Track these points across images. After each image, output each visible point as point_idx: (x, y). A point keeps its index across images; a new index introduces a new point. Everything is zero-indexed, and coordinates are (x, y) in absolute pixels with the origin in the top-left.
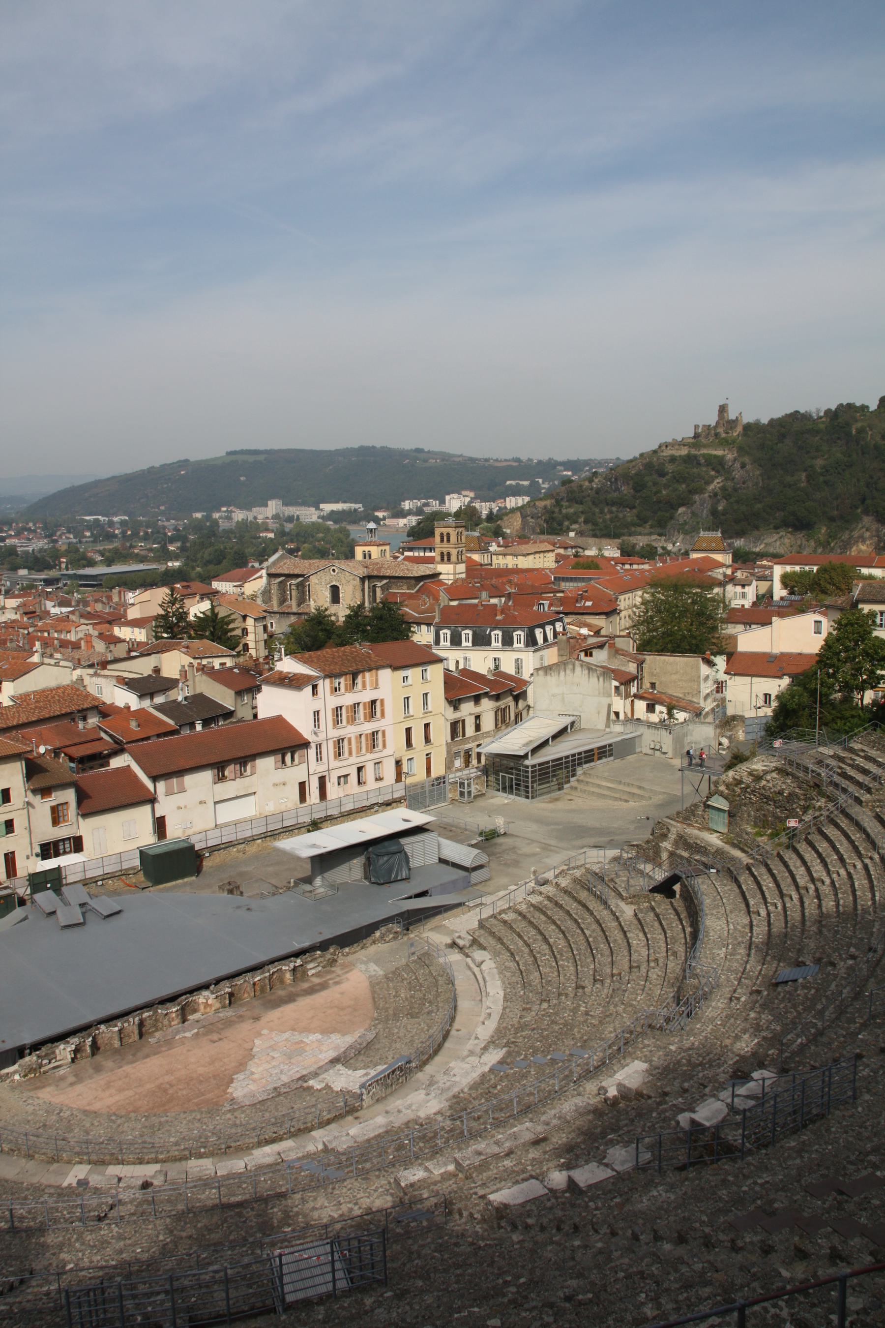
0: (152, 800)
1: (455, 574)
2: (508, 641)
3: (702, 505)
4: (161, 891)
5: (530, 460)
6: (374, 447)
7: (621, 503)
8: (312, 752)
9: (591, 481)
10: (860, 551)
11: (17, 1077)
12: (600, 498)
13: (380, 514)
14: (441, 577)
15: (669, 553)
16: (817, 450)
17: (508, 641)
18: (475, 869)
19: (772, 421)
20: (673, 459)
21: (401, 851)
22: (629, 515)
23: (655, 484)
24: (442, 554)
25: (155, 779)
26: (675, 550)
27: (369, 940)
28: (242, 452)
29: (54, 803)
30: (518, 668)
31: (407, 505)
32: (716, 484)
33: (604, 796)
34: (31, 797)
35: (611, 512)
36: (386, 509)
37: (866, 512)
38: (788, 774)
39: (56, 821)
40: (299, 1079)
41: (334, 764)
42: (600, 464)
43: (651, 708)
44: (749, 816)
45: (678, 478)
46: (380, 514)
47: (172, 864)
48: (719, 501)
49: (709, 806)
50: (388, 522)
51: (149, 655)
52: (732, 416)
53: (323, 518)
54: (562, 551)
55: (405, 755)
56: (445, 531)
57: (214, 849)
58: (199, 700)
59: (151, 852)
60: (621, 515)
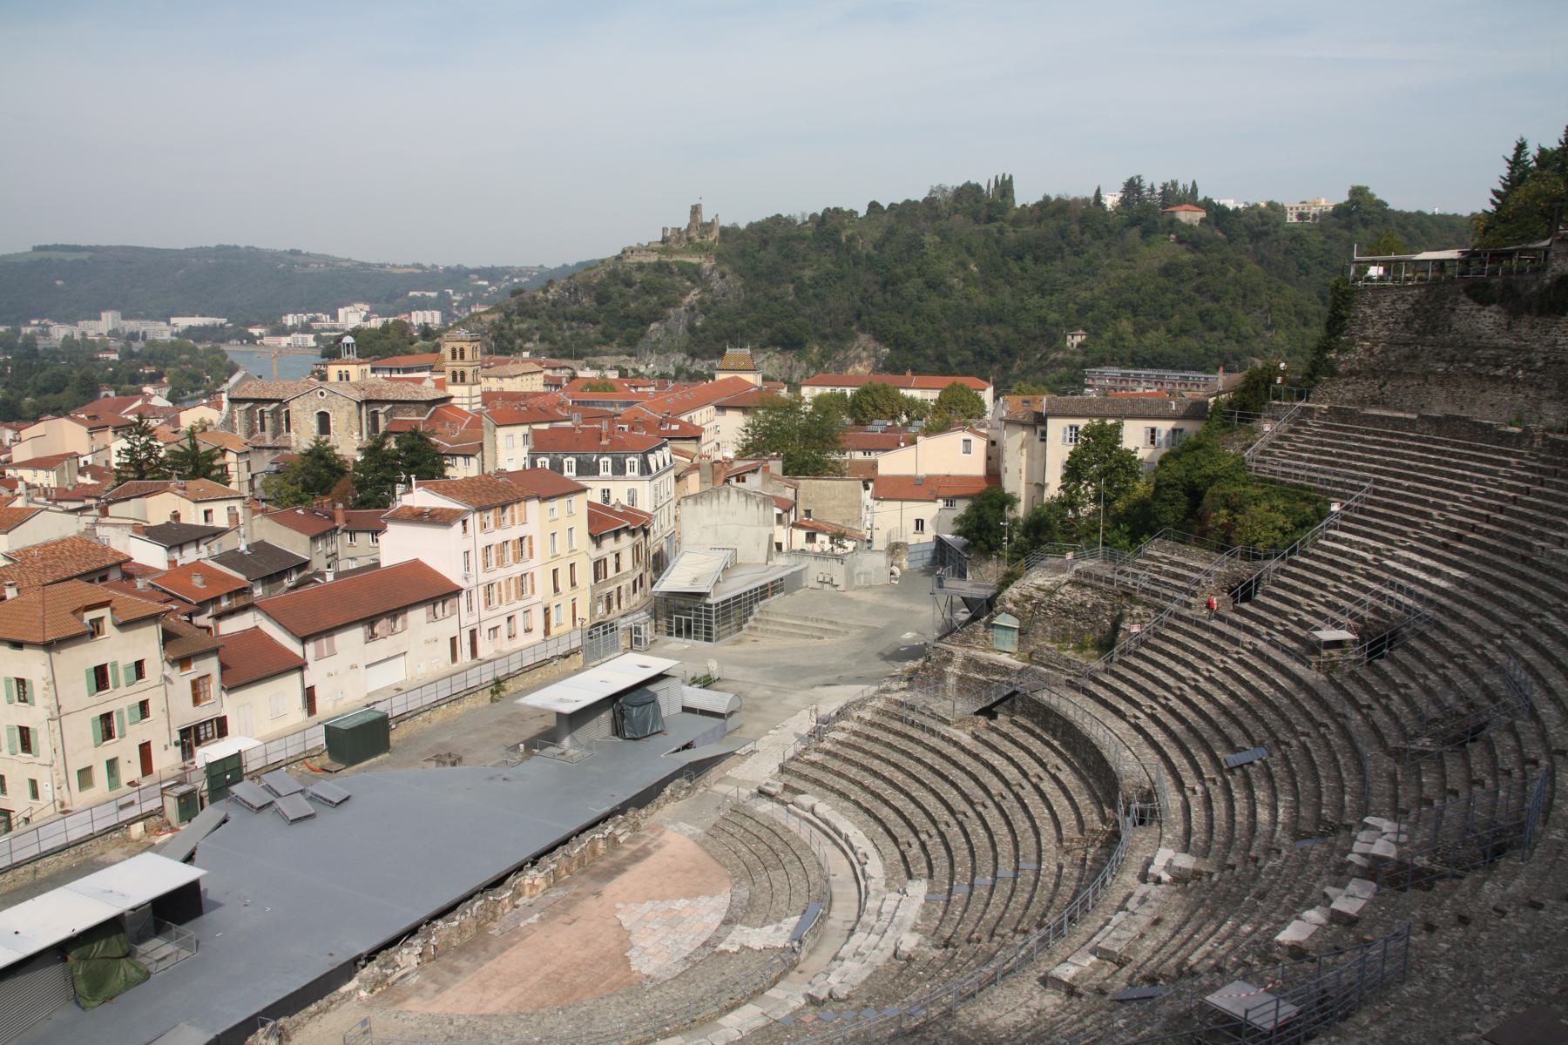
0: (301, 667)
1: (471, 397)
2: (619, 469)
3: (677, 320)
4: (365, 770)
5: (434, 266)
6: (236, 247)
7: (582, 318)
8: (463, 599)
9: (546, 291)
10: (857, 373)
11: (363, 994)
12: (557, 313)
13: (256, 331)
14: (453, 401)
15: (641, 375)
16: (805, 260)
17: (619, 469)
18: (731, 714)
19: (751, 225)
20: (641, 267)
21: (653, 700)
22: (593, 332)
23: (621, 295)
24: (454, 374)
25: (304, 640)
26: (648, 372)
27: (660, 799)
28: (56, 248)
29: (194, 677)
30: (633, 500)
31: (290, 320)
32: (693, 296)
33: (792, 634)
34: (168, 671)
35: (571, 328)
36: (264, 325)
37: (863, 329)
38: (1085, 586)
39: (196, 700)
40: (704, 944)
41: (485, 614)
42: (521, 272)
43: (811, 538)
44: (1045, 631)
45: (648, 289)
46: (256, 331)
47: (359, 740)
48: (696, 317)
49: (994, 626)
50: (266, 340)
51: (128, 499)
52: (706, 218)
53: (177, 334)
54: (549, 372)
55: (553, 601)
56: (458, 346)
57: (401, 718)
58: (260, 548)
59: (344, 726)
60: (583, 332)
